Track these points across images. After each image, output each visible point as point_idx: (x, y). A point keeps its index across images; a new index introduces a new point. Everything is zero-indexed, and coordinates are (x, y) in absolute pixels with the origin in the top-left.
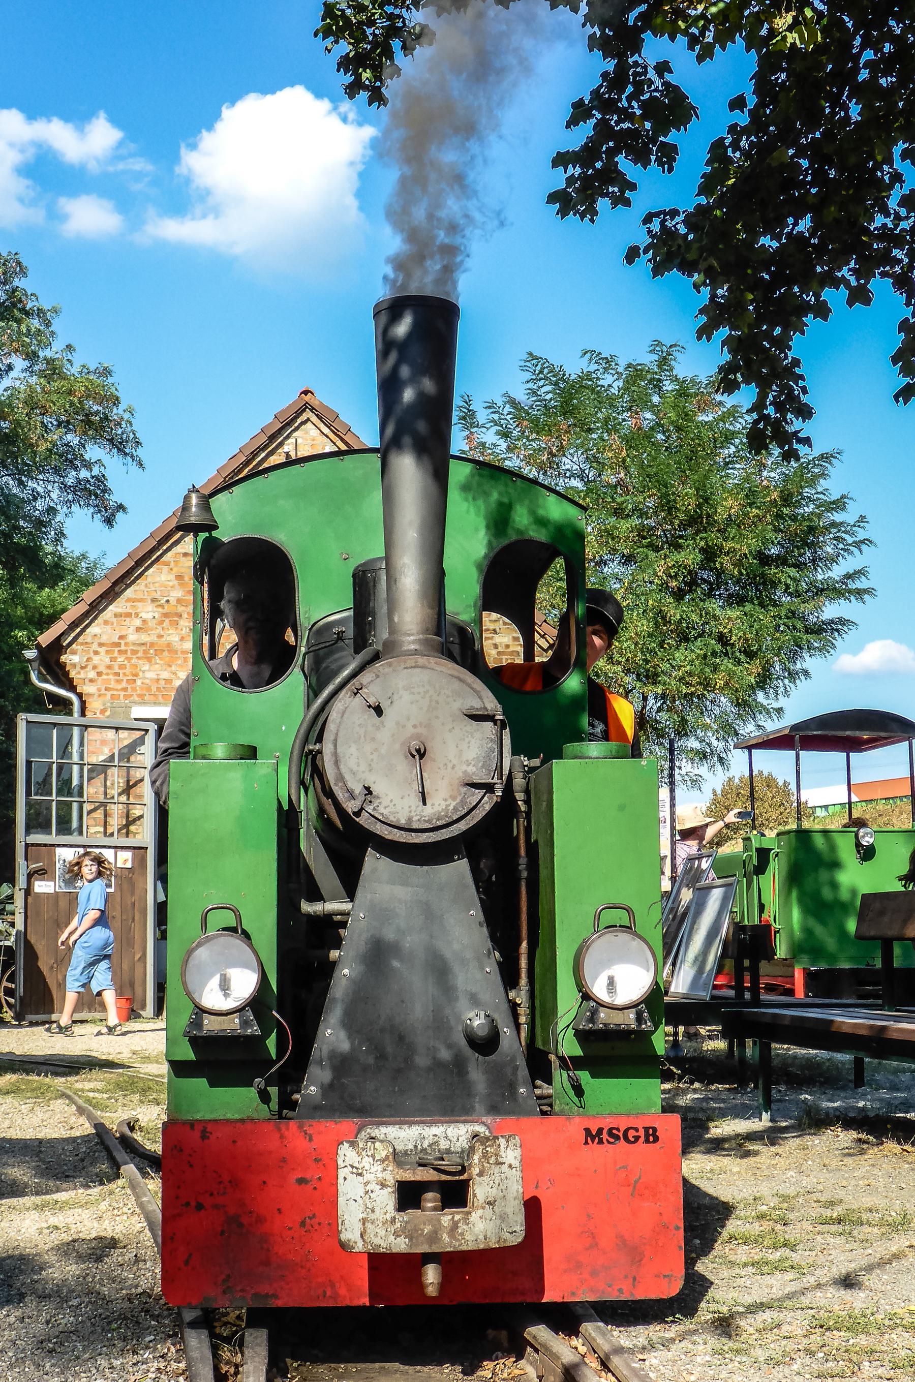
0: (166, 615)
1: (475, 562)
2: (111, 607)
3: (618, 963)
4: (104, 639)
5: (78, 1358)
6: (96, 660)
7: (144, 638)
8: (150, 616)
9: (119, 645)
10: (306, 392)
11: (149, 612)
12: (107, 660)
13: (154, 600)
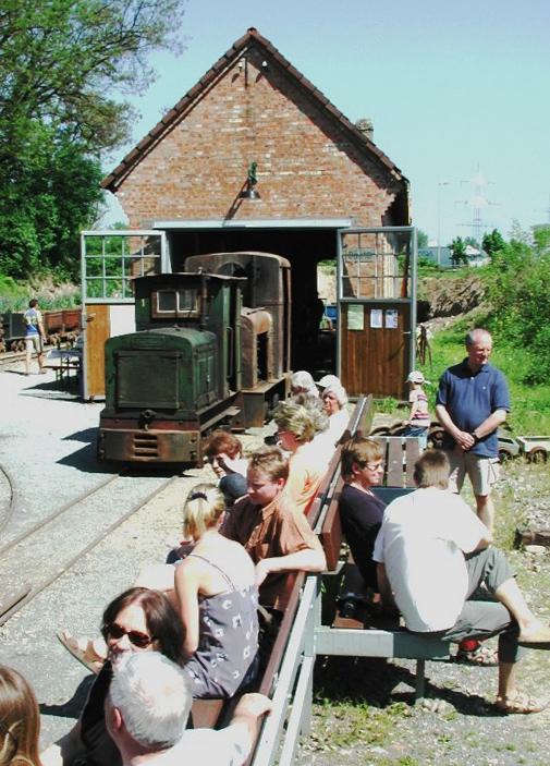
0: (173, 167)
1: (203, 587)
2: (141, 164)
3: (418, 617)
4: (138, 182)
5: (286, 192)
6: (134, 195)
7: (160, 181)
8: (163, 168)
9: (145, 185)
10: (252, 29)
11: (162, 166)
12: (140, 195)
13: (165, 158)
